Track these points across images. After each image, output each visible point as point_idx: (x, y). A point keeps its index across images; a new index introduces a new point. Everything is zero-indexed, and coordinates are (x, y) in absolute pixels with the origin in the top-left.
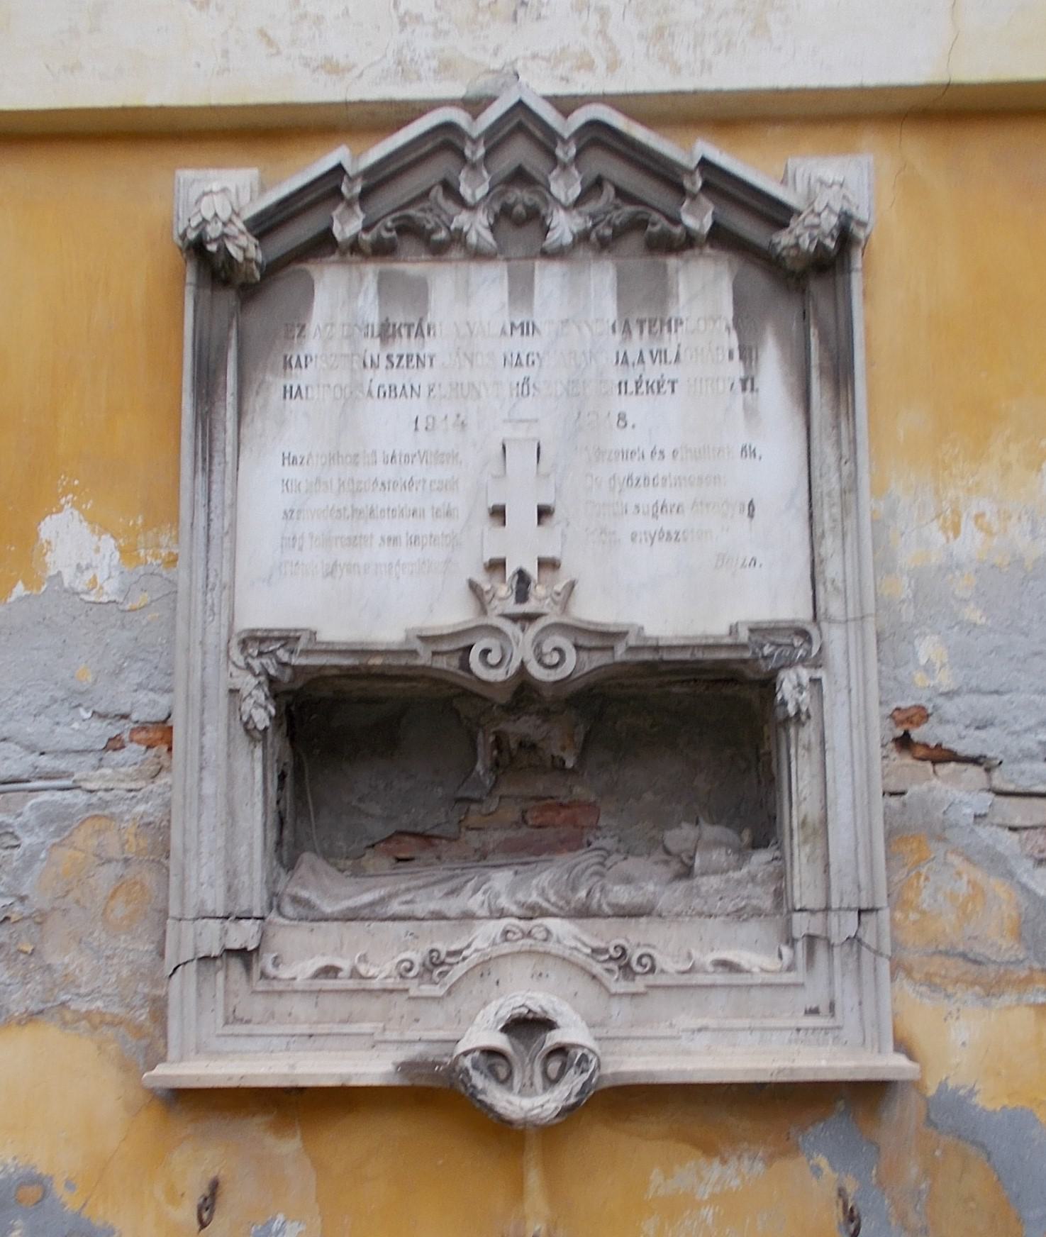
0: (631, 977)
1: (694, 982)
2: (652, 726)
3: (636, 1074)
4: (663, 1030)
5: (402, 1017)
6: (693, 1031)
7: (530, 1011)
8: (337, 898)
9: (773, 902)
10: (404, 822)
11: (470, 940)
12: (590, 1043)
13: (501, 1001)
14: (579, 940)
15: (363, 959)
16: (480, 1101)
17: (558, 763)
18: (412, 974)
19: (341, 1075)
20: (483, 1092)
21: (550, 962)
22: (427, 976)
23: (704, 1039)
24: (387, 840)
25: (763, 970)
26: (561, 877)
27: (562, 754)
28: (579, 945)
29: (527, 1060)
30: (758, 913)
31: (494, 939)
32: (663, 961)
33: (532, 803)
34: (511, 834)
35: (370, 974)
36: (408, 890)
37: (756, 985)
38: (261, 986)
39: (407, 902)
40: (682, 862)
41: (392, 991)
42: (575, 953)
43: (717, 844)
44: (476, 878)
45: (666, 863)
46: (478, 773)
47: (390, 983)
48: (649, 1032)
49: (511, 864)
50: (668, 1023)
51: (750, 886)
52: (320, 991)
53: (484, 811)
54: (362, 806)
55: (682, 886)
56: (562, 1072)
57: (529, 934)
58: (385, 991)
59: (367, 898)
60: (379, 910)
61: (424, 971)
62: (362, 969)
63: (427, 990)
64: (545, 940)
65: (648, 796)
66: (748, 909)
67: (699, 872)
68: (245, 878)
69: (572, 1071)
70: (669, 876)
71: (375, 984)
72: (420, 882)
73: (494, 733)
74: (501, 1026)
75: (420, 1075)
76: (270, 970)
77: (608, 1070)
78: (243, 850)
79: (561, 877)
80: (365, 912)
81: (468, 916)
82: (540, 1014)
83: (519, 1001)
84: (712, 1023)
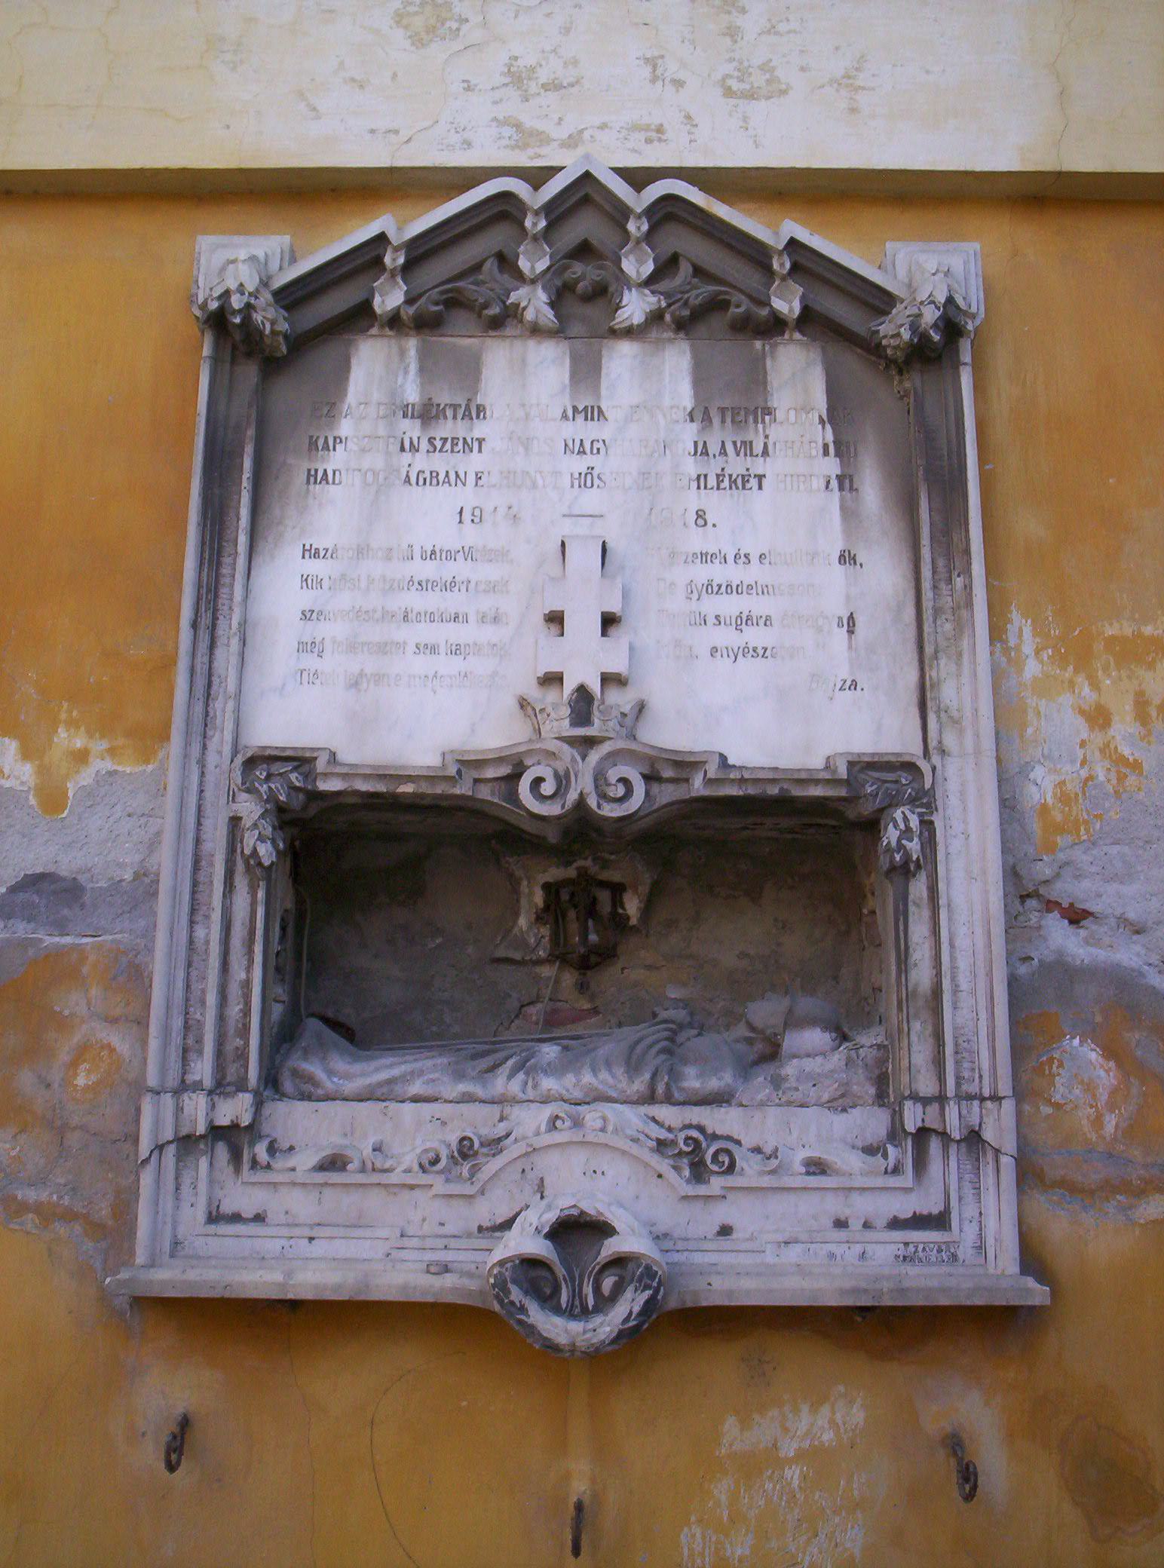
59: (383, 1076)
71: (394, 1178)
80: (378, 1093)
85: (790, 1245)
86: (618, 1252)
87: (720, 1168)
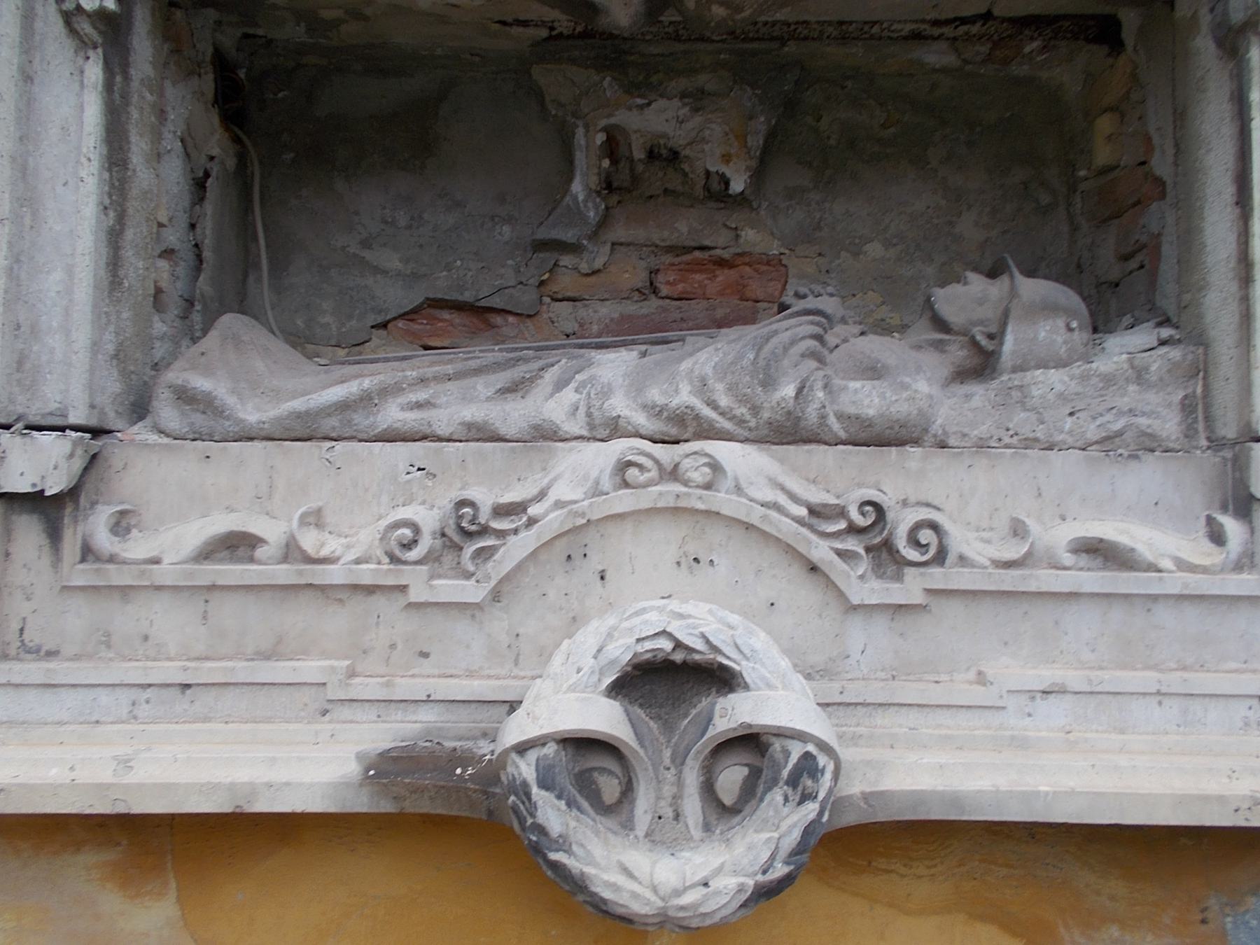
0: (891, 569)
1: (1033, 587)
2: (884, 126)
3: (919, 797)
4: (962, 690)
5: (393, 646)
6: (1032, 694)
7: (678, 645)
8: (278, 395)
9: (1180, 424)
10: (441, 286)
11: (546, 481)
12: (817, 725)
13: (611, 621)
14: (783, 489)
15: (315, 519)
16: (556, 866)
17: (715, 186)
18: (413, 554)
19: (232, 787)
20: (563, 844)
21: (716, 534)
22: (448, 559)
23: (1056, 712)
24: (410, 315)
25: (1183, 566)
26: (741, 356)
27: (724, 169)
28: (783, 500)
29: (667, 754)
30: (1149, 444)
31: (597, 483)
32: (961, 540)
33: (668, 259)
34: (631, 308)
35: (324, 552)
36: (423, 381)
37: (1167, 597)
38: (81, 575)
39: (419, 406)
40: (974, 343)
41: (371, 590)
42: (774, 514)
43: (1049, 309)
44: (564, 361)
45: (939, 346)
46: (575, 198)
47: (367, 574)
48: (935, 695)
49: (634, 343)
50: (972, 675)
51: (1132, 388)
52: (212, 588)
53: (584, 267)
54: (367, 254)
55: (980, 394)
56: (750, 791)
57: (673, 473)
58: (355, 588)
59: (336, 393)
60: (361, 420)
61: (444, 546)
62: (309, 541)
63: (450, 589)
64: (708, 486)
65: (875, 249)
66: (1128, 436)
67: (1010, 364)
68: (55, 341)
69: (777, 795)
70: (945, 372)
71: (335, 575)
72: (450, 369)
73: (605, 129)
74: (608, 680)
75: (416, 790)
76: (104, 540)
77: (854, 787)
78: (53, 281)
79: (741, 356)
80: (331, 424)
81: (545, 434)
82: (703, 654)
83: (653, 621)
84: (1074, 678)
85: (1051, 697)
86: (750, 726)
87: (923, 554)
